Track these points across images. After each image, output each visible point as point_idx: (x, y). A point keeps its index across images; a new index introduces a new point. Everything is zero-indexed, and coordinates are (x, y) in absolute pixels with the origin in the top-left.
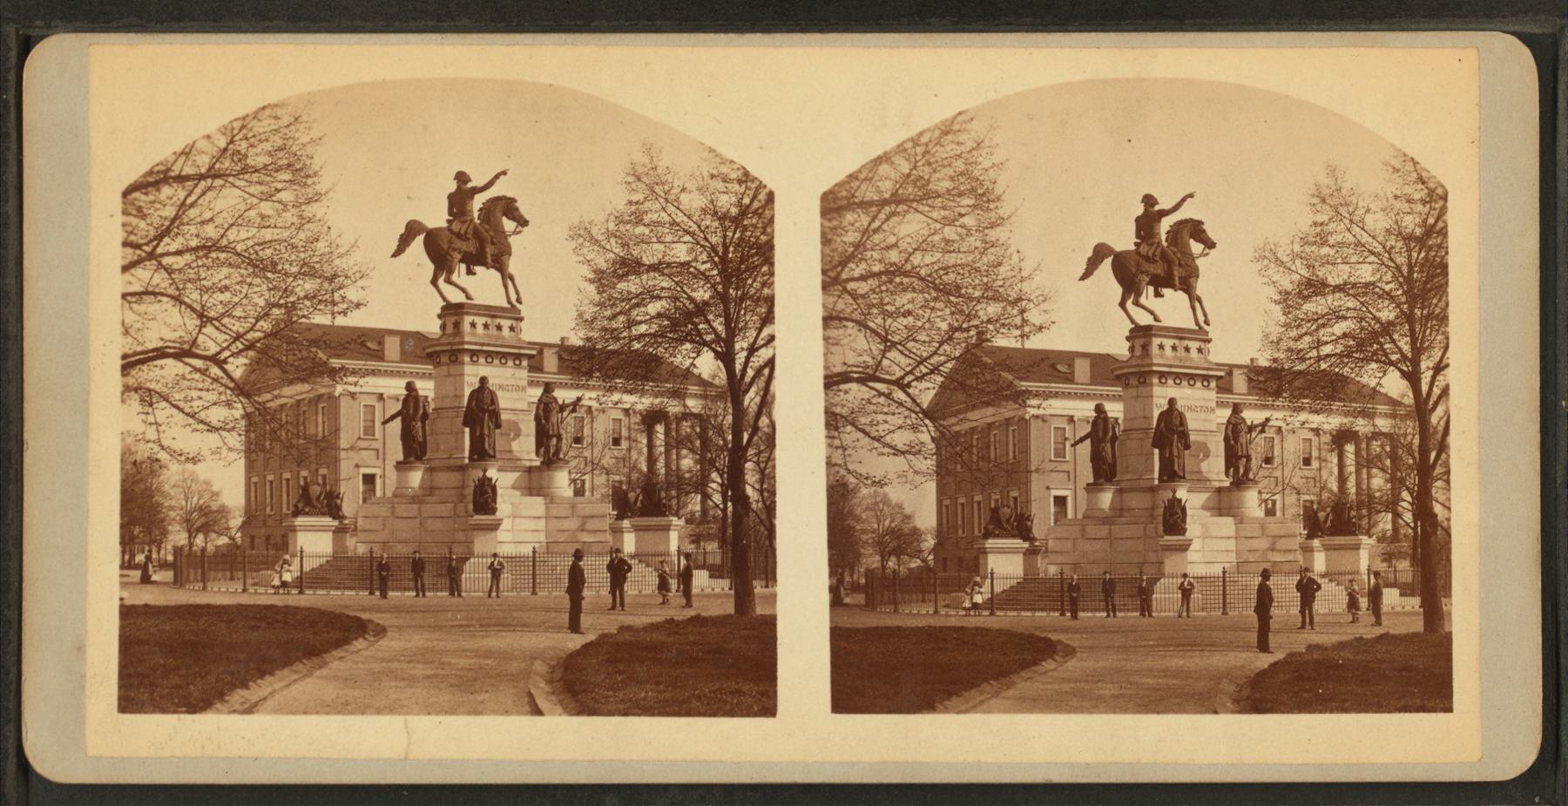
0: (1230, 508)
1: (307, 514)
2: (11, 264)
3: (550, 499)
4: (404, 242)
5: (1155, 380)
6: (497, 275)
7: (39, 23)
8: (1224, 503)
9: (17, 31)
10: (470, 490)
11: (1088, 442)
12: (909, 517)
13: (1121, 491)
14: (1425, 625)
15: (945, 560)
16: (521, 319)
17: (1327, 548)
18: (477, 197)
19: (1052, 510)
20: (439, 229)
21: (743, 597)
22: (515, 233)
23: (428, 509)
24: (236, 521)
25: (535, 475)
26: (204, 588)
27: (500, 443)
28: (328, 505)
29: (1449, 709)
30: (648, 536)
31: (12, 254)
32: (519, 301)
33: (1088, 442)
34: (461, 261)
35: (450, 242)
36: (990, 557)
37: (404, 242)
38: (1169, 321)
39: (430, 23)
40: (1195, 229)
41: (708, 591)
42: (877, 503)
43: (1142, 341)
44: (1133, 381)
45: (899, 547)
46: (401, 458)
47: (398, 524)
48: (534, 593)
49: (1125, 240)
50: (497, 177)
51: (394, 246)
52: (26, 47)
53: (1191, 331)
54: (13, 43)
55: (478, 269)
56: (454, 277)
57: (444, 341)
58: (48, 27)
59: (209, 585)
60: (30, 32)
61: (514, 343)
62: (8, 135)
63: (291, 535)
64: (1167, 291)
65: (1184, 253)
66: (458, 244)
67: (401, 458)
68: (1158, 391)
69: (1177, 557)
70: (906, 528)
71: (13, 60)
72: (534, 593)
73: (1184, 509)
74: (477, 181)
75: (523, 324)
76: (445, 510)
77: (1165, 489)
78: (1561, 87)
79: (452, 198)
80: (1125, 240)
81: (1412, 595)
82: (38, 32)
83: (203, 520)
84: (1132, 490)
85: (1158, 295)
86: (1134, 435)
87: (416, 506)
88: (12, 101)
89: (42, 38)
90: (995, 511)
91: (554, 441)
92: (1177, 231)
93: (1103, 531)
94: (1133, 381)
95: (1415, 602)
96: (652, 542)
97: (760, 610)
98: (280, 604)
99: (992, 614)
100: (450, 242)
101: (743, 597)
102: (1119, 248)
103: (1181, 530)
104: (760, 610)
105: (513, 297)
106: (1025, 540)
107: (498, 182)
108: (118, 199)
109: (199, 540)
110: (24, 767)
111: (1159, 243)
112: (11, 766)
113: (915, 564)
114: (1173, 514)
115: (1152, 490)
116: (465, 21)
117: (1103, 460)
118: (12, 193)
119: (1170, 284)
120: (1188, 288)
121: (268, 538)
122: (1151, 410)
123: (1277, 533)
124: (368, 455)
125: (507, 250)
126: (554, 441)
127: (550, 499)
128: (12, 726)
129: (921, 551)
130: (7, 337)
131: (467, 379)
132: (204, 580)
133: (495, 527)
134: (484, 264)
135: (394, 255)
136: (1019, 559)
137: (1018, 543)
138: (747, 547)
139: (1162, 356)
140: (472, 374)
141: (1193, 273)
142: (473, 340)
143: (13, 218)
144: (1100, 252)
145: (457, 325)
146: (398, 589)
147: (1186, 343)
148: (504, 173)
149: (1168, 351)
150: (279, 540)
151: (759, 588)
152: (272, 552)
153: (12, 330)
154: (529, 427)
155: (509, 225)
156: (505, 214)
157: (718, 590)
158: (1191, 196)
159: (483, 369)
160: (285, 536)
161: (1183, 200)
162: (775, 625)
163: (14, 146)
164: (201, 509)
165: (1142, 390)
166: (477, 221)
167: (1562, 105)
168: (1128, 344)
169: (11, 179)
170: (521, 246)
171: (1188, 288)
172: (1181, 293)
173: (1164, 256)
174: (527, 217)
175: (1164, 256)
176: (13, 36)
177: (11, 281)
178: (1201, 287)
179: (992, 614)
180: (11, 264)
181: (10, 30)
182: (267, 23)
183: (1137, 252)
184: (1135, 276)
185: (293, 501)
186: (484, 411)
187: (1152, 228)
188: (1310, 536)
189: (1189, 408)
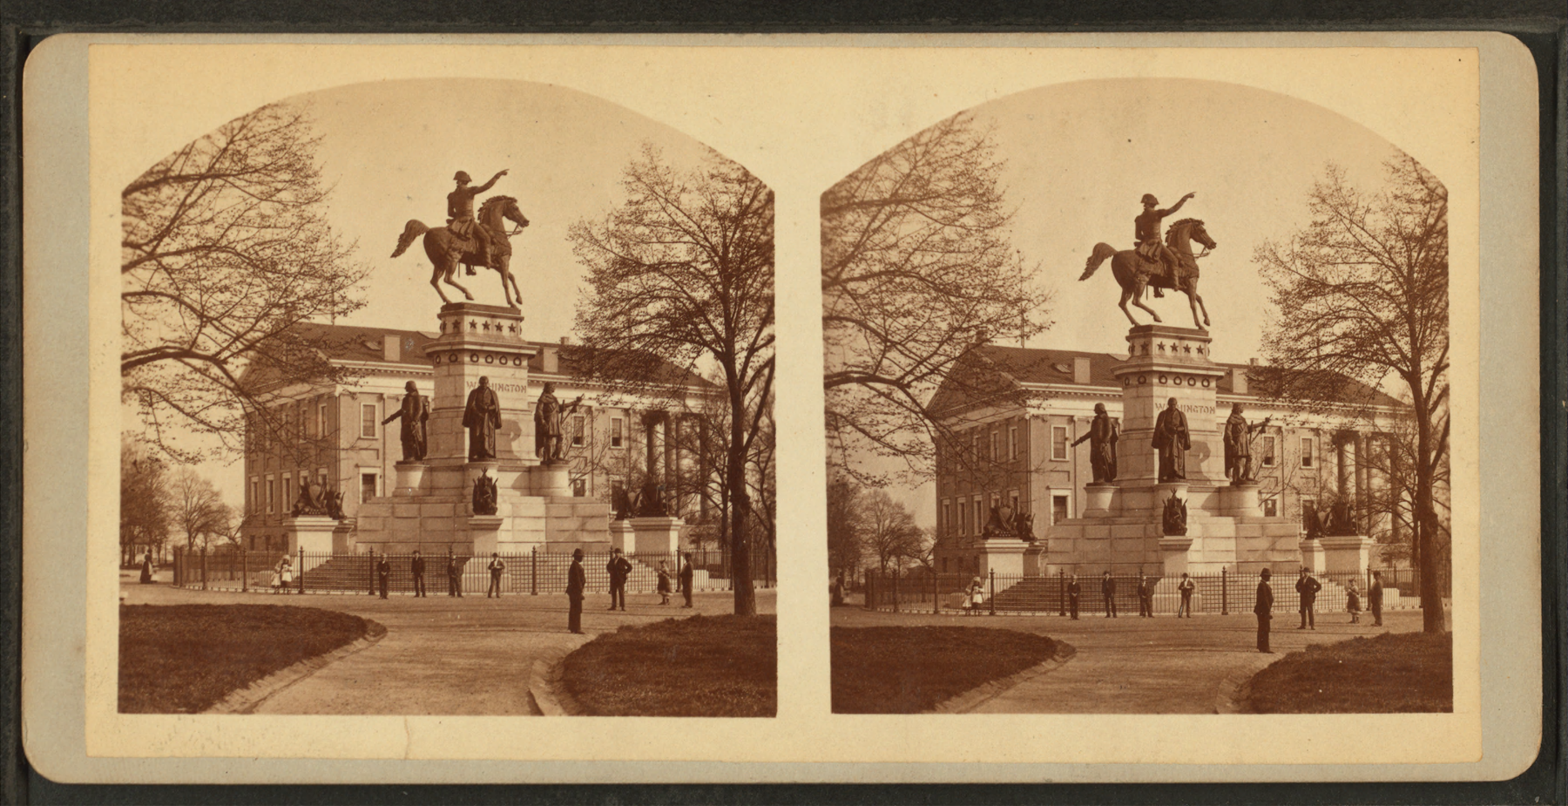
0: (1230, 508)
1: (307, 514)
2: (11, 264)
3: (550, 499)
4: (404, 242)
5: (1155, 380)
6: (497, 275)
7: (39, 23)
8: (1223, 503)
9: (17, 31)
10: (470, 490)
11: (1088, 442)
12: (909, 517)
13: (1121, 491)
14: (1425, 625)
15: (945, 560)
16: (521, 319)
17: (1327, 548)
18: (477, 197)
19: (1052, 509)
20: (1127, 252)
21: (743, 597)
22: (515, 233)
23: (428, 509)
24: (236, 522)
25: (535, 475)
26: (204, 588)
27: (500, 443)
28: (328, 506)
29: (1449, 709)
30: (649, 536)
31: (12, 254)
32: (519, 301)
33: (1088, 442)
34: (461, 261)
35: (450, 242)
36: (990, 557)
37: (404, 242)
38: (1168, 321)
39: (431, 23)
40: (1195, 229)
41: (708, 591)
42: (877, 503)
43: (1142, 341)
44: (1133, 381)
45: (899, 547)
46: (401, 458)
47: (400, 524)
48: (534, 593)
49: (1125, 240)
50: (497, 177)
51: (1082, 271)
52: (26, 47)
53: (1191, 331)
54: (13, 43)
55: (478, 269)
56: (455, 278)
57: (444, 341)
58: (48, 26)
59: (209, 585)
60: (30, 32)
61: (514, 343)
62: (8, 135)
63: (291, 535)
64: (1166, 291)
65: (495, 231)
66: (458, 244)
67: (401, 458)
68: (1158, 391)
69: (1178, 557)
70: (906, 528)
71: (13, 61)
72: (534, 593)
73: (1184, 509)
74: (477, 181)
75: (523, 324)
76: (446, 510)
77: (1166, 489)
78: (1561, 87)
79: (451, 198)
80: (1125, 240)
81: (1412, 595)
82: (38, 32)
83: (203, 520)
84: (1132, 490)
85: (1158, 295)
86: (1134, 435)
87: (416, 506)
88: (12, 101)
89: (42, 38)
90: (995, 511)
91: (554, 441)
92: (1177, 231)
93: (1103, 531)
94: (1133, 381)
95: (1415, 602)
96: (652, 542)
97: (760, 610)
98: (280, 604)
99: (992, 614)
100: (450, 242)
101: (743, 597)
102: (1119, 248)
103: (1181, 531)
104: (760, 610)
105: (513, 297)
106: (1025, 540)
107: (498, 182)
108: (118, 199)
109: (199, 540)
110: (24, 766)
111: (1159, 243)
112: (11, 766)
113: (915, 564)
114: (1173, 514)
115: (1152, 490)
116: (465, 21)
117: (1103, 460)
118: (12, 193)
119: (1170, 284)
120: (1188, 288)
121: (268, 538)
122: (1151, 410)
123: (1278, 533)
124: (368, 455)
125: (507, 250)
126: (554, 441)
127: (550, 499)
128: (12, 726)
129: (921, 551)
130: (7, 337)
131: (467, 379)
132: (204, 580)
133: (495, 527)
134: (484, 263)
135: (394, 255)
136: (1019, 559)
137: (1018, 543)
138: (747, 547)
139: (1162, 356)
140: (472, 374)
141: (1193, 273)
142: (1161, 361)
143: (13, 219)
144: (1100, 252)
145: (457, 325)
146: (397, 589)
147: (1186, 343)
148: (504, 173)
149: (1168, 351)
150: (279, 540)
151: (759, 588)
152: (272, 552)
153: (12, 330)
154: (529, 427)
155: (509, 225)
156: (505, 214)
157: (718, 590)
158: (1191, 196)
159: (483, 369)
160: (285, 536)
161: (1183, 200)
162: (775, 625)
163: (14, 146)
164: (201, 509)
165: (1143, 390)
166: (477, 221)
167: (1562, 104)
168: (1128, 344)
169: (11, 179)
170: (521, 245)
171: (1188, 288)
172: (492, 271)
173: (476, 234)
174: (527, 217)
175: (1164, 256)
176: (13, 36)
177: (11, 281)
178: (1201, 288)
179: (992, 614)
180: (11, 264)
181: (10, 30)
182: (267, 23)
183: (1137, 252)
184: (1135, 276)
185: (293, 501)
186: (484, 411)
187: (1152, 228)
188: (1310, 536)
189: (1189, 408)
